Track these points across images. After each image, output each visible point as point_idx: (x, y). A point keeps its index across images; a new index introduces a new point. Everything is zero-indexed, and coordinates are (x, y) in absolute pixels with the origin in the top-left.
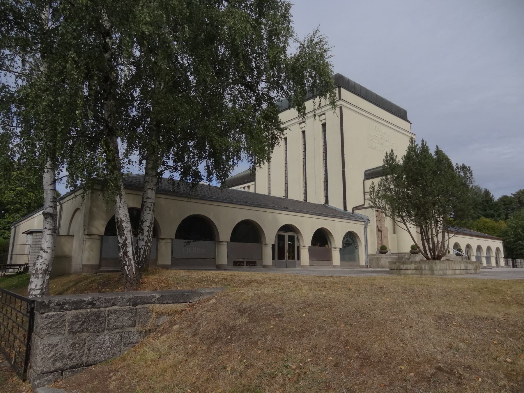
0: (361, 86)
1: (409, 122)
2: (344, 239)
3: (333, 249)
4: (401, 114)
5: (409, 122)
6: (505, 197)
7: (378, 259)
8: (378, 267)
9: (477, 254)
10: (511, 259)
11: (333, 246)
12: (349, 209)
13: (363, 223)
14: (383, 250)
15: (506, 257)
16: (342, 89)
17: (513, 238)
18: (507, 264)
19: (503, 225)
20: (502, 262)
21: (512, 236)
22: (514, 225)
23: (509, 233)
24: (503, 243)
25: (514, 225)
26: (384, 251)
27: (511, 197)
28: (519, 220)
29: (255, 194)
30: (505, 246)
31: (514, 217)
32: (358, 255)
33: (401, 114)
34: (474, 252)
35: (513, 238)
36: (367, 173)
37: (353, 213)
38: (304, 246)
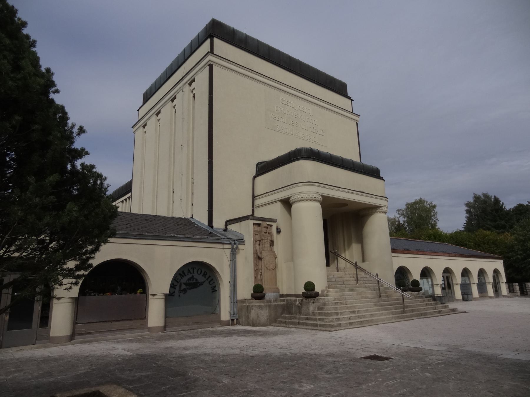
0: (258, 41)
1: (349, 98)
2: (175, 279)
3: (472, 284)
4: (339, 88)
5: (349, 98)
6: (520, 206)
7: (248, 309)
8: (248, 325)
9: (462, 280)
10: (517, 284)
11: (454, 283)
12: (218, 223)
13: (230, 246)
14: (258, 293)
15: (510, 281)
16: (216, 40)
17: (521, 255)
18: (511, 290)
19: (508, 238)
20: (504, 288)
21: (519, 253)
22: (521, 238)
23: (516, 248)
24: (504, 263)
25: (521, 238)
26: (259, 294)
27: (527, 205)
28: (528, 231)
29: (130, 214)
30: (507, 267)
31: (521, 227)
32: (51, 315)
33: (339, 88)
34: (458, 279)
35: (521, 255)
36: (260, 166)
37: (226, 230)
38: (457, 284)
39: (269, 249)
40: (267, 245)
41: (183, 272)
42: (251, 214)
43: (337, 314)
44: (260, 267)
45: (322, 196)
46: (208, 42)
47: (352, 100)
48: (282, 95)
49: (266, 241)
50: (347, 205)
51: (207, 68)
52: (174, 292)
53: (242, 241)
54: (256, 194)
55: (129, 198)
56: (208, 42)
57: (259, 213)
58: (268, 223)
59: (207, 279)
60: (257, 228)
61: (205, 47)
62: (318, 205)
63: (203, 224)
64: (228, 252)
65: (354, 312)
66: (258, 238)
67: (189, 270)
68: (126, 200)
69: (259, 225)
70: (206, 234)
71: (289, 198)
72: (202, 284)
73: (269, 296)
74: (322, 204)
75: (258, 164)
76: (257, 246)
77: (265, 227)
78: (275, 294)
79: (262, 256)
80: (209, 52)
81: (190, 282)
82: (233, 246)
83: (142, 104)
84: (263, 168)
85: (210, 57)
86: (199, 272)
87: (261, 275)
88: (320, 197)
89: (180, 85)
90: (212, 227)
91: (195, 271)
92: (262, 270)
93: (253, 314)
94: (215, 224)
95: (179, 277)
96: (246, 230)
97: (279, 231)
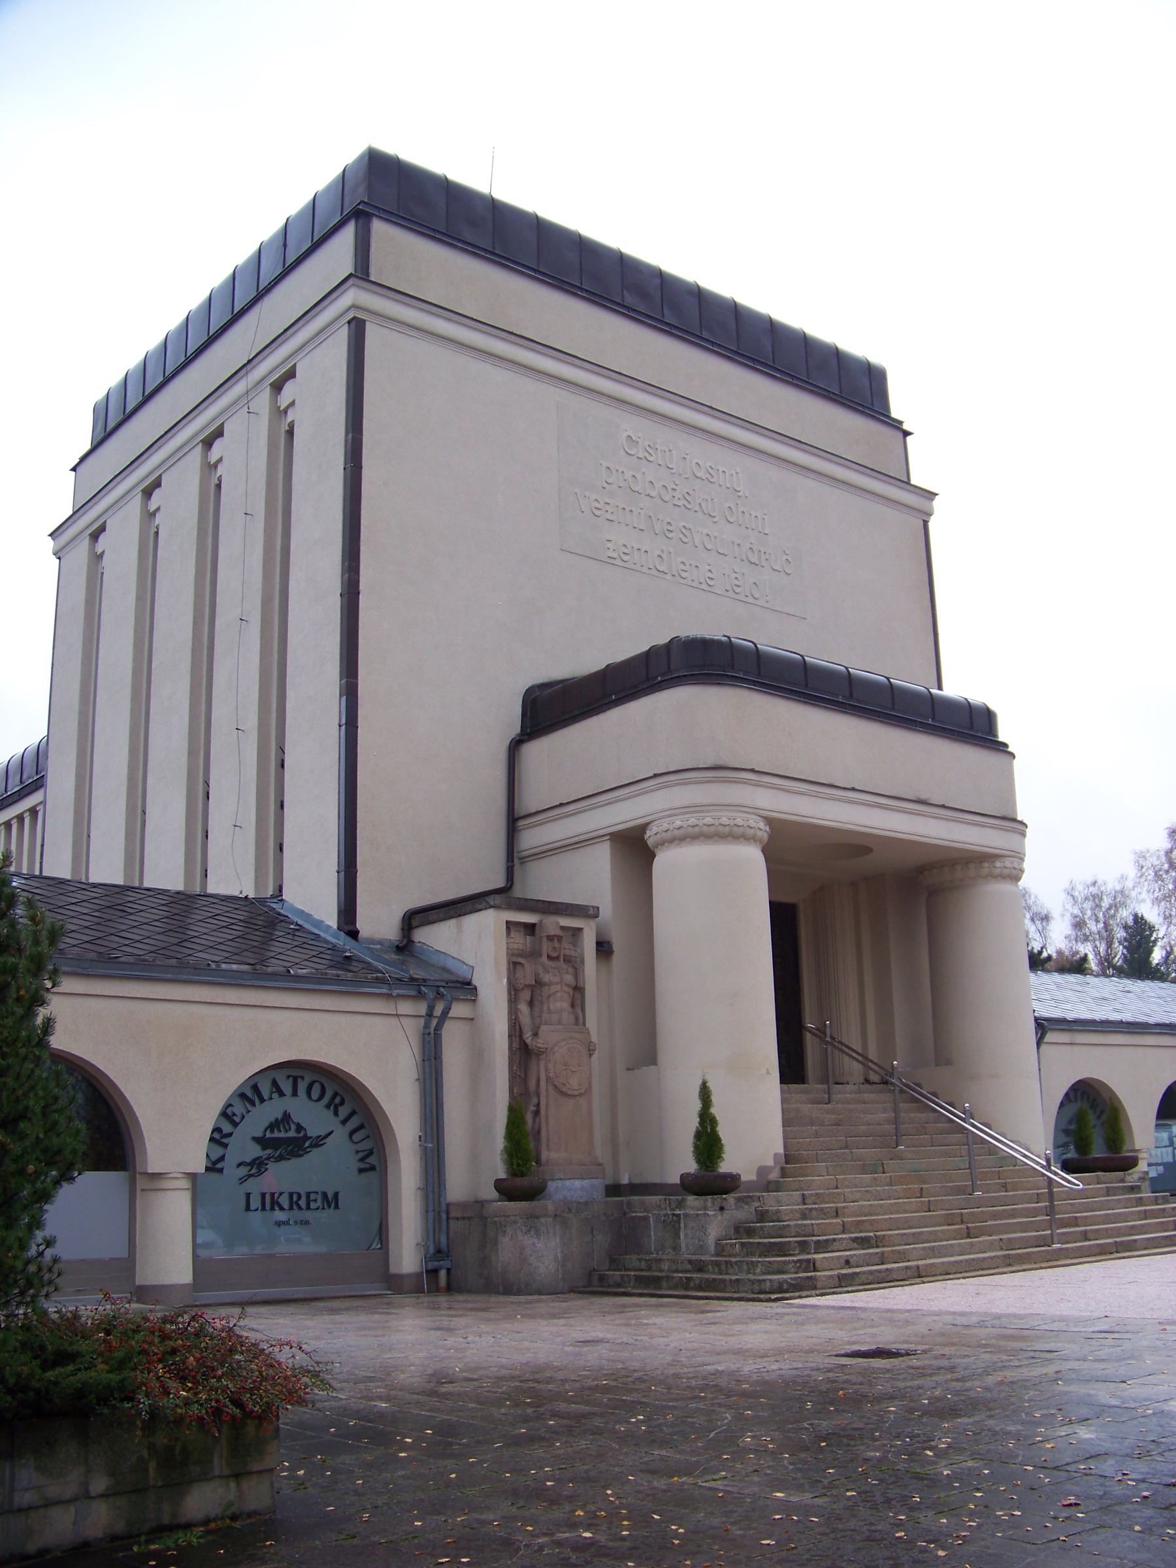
5: (896, 425)
14: (523, 1179)
33: (855, 387)
39: (567, 1017)
40: (560, 1003)
41: (255, 1088)
42: (500, 883)
43: (803, 1246)
44: (532, 1084)
45: (769, 821)
46: (348, 234)
47: (906, 434)
48: (630, 425)
49: (553, 989)
50: (867, 850)
51: (342, 335)
52: (222, 1158)
53: (465, 988)
54: (520, 810)
55: (33, 812)
56: (348, 234)
57: (543, 882)
58: (566, 922)
59: (344, 1122)
60: (521, 941)
61: (339, 253)
62: (753, 859)
63: (319, 923)
64: (412, 1028)
65: (863, 1242)
66: (526, 976)
67: (275, 1083)
68: (20, 818)
69: (530, 929)
70: (343, 965)
71: (644, 828)
72: (318, 1142)
73: (570, 1187)
74: (769, 853)
75: (530, 692)
76: (523, 1008)
77: (550, 938)
78: (586, 1182)
79: (540, 1043)
80: (350, 276)
81: (276, 1134)
82: (431, 1008)
83: (88, 447)
84: (550, 708)
85: (351, 296)
86: (315, 1093)
87: (537, 1113)
88: (762, 825)
89: (239, 388)
90: (354, 934)
91: (302, 1087)
92: (538, 1095)
93: (506, 1252)
94: (364, 925)
95: (239, 1108)
96: (477, 946)
97: (604, 948)
